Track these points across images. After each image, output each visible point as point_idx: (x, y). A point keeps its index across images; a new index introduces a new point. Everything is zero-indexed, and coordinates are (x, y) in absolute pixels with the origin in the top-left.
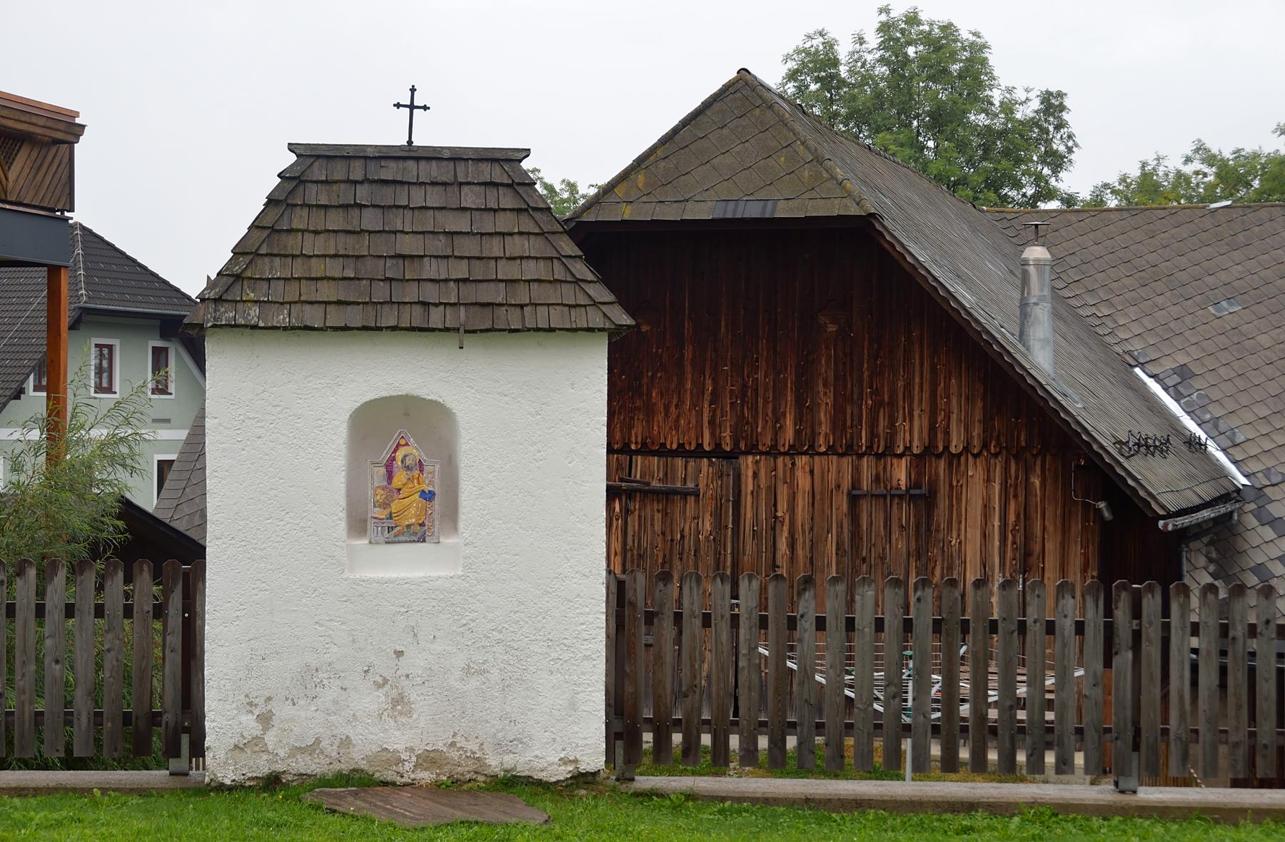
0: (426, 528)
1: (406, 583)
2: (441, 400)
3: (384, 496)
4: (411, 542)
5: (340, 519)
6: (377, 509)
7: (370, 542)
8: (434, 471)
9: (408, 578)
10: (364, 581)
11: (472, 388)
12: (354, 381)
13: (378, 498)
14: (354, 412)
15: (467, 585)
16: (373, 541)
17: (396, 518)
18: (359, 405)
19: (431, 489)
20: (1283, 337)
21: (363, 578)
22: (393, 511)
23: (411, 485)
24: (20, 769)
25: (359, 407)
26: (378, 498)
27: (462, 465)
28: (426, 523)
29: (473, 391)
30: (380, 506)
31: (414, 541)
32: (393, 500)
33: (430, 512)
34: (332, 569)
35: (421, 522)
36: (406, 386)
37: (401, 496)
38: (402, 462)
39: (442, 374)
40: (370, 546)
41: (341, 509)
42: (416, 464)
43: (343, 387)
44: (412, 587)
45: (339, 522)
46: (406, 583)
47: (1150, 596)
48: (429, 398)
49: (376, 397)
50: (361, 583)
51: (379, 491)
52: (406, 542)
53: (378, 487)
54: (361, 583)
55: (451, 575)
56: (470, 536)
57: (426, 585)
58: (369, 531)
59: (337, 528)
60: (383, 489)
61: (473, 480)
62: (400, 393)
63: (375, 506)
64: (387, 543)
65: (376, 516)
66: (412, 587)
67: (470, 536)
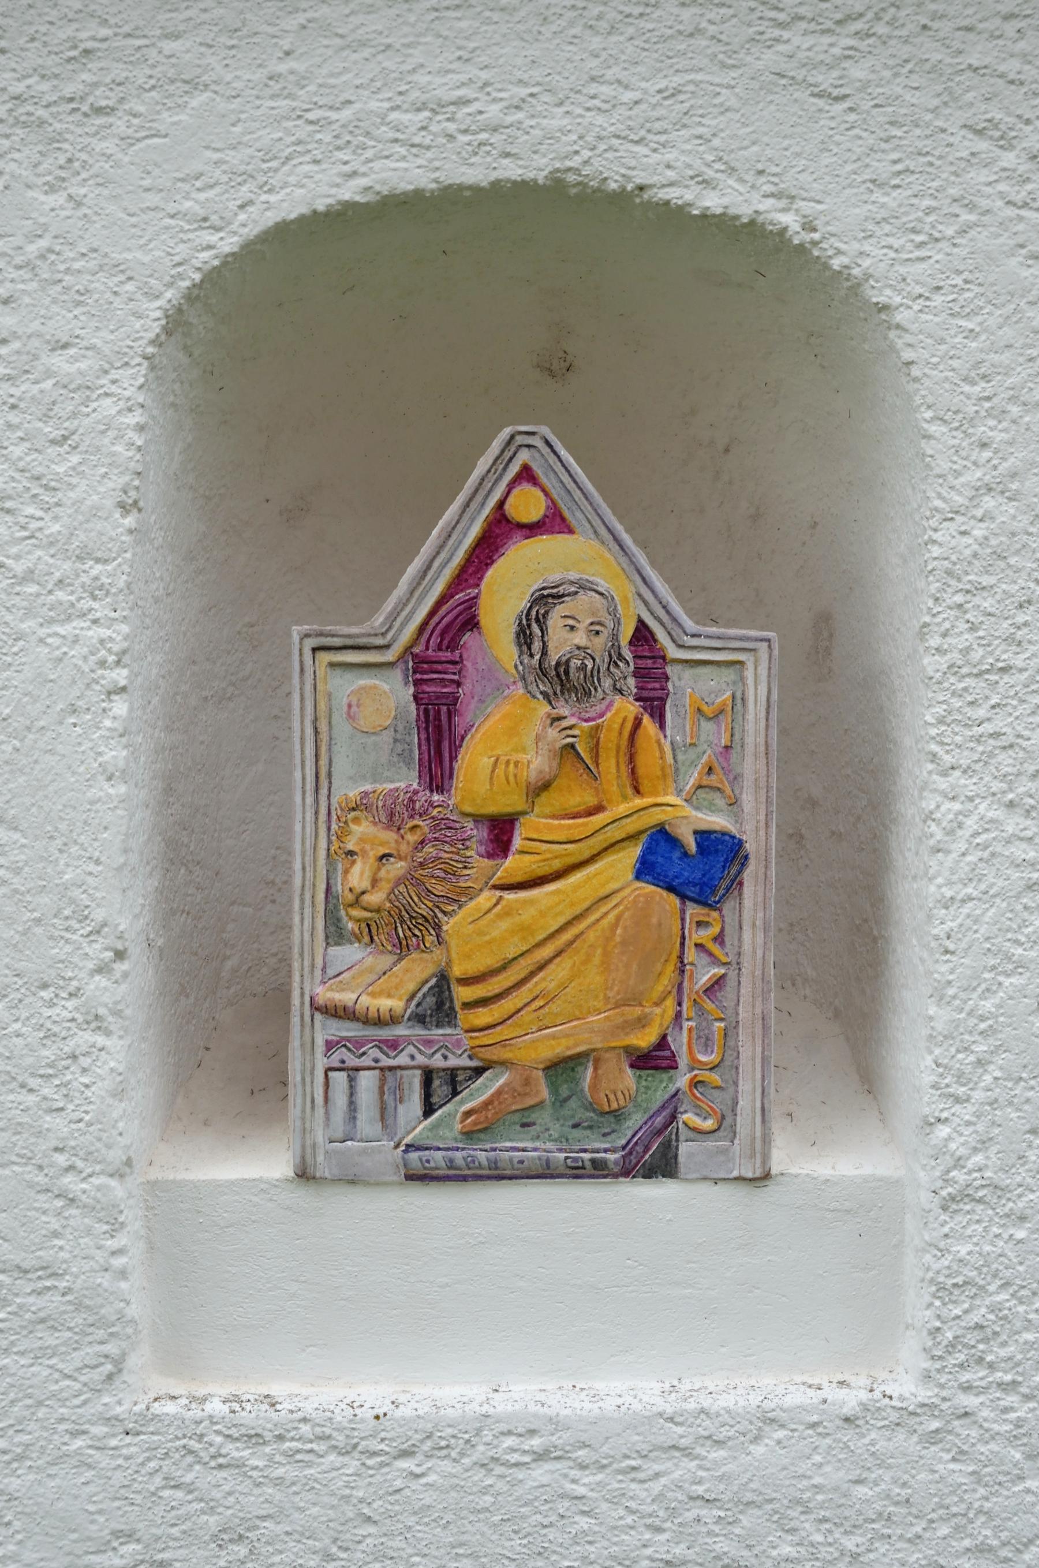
0: (682, 1080)
1: (541, 1456)
2: (789, 220)
3: (397, 868)
4: (576, 1172)
5: (96, 1022)
6: (350, 953)
7: (304, 1175)
8: (738, 701)
9: (556, 1424)
10: (255, 1439)
11: (1005, 142)
12: (194, 85)
13: (358, 876)
14: (192, 296)
15: (960, 1472)
16: (323, 1167)
17: (483, 1016)
18: (229, 244)
19: (718, 821)
20: (5, 385)
21: (250, 1417)
22: (457, 971)
23: (582, 797)
24: (481, 579)
25: (231, 261)
26: (358, 876)
27: (933, 664)
28: (680, 1043)
29: (1008, 159)
30: (369, 933)
31: (598, 1170)
32: (459, 898)
33: (705, 975)
34: (39, 1355)
35: (645, 1040)
36: (557, 121)
37: (513, 865)
38: (524, 637)
39: (796, 38)
40: (303, 1197)
41: (98, 951)
42: (615, 658)
43: (120, 124)
44: (585, 1484)
45: (86, 1038)
46: (541, 1456)
47: (892, 334)
48: (712, 202)
49: (349, 192)
50: (234, 1451)
51: (362, 829)
52: (546, 1173)
53: (361, 806)
54: (234, 1451)
55: (850, 1400)
56: (984, 1144)
57: (683, 1469)
58: (295, 1093)
59: (73, 1076)
60: (392, 821)
61: (1005, 761)
62: (512, 171)
63: (336, 934)
64: (411, 1177)
65: (347, 998)
66: (585, 1484)
67: (984, 1144)
